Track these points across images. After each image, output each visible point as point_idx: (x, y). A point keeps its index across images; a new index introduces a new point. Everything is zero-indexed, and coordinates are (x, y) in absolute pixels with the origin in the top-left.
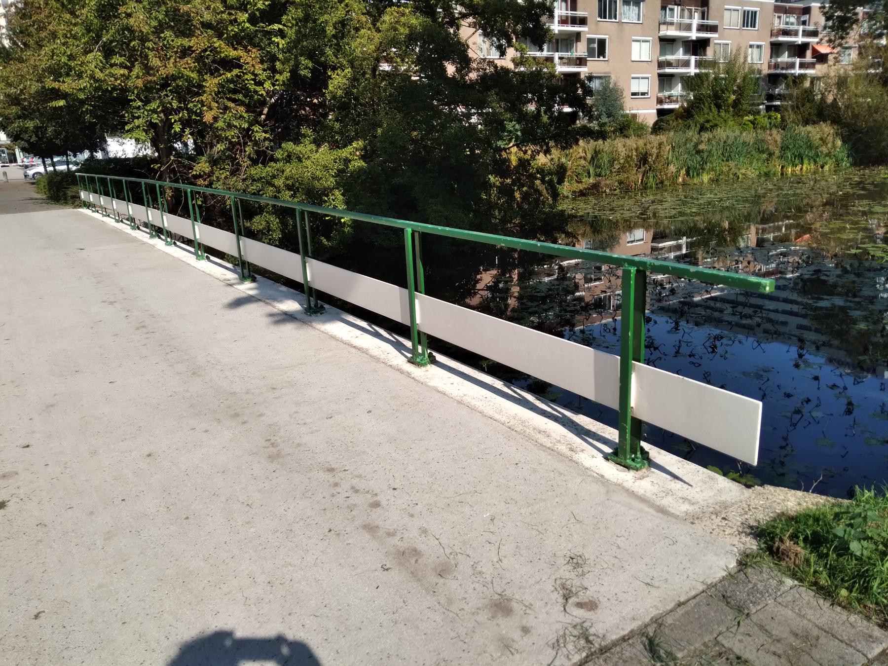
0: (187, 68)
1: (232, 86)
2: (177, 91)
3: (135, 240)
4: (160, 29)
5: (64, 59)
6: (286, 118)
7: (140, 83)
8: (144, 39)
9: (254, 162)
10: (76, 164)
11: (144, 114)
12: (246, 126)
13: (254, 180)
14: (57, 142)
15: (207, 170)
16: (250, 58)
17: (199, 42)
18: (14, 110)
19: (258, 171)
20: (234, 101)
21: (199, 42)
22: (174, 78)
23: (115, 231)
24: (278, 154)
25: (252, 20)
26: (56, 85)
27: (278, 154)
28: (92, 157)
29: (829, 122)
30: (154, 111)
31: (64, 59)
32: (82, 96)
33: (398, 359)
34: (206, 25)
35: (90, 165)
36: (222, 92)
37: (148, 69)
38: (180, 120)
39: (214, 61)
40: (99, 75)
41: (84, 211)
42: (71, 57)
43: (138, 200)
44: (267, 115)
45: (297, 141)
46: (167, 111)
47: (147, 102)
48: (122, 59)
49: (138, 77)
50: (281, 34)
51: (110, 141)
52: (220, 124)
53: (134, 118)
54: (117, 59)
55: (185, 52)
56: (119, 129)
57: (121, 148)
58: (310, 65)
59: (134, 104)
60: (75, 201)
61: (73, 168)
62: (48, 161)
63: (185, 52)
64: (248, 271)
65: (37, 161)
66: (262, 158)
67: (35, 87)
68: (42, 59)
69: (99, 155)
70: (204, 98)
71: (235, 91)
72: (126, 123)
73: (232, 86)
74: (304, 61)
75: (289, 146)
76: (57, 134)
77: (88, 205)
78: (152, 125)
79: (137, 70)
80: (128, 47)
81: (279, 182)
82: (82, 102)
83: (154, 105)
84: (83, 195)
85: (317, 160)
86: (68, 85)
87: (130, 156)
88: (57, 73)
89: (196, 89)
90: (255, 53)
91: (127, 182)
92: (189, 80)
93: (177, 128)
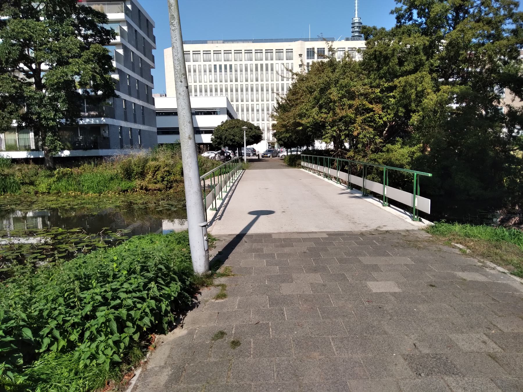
0: (350, 113)
1: (369, 119)
2: (345, 122)
3: (318, 178)
4: (341, 98)
5: (305, 111)
6: (397, 131)
7: (331, 120)
8: (335, 102)
9: (373, 152)
10: (300, 151)
11: (331, 131)
12: (372, 136)
13: (371, 160)
14: (295, 142)
15: (353, 155)
16: (377, 108)
17: (356, 102)
18: (284, 130)
19: (373, 156)
20: (369, 126)
21: (356, 102)
22: (345, 117)
23: (312, 176)
24: (384, 149)
25: (382, 91)
26: (300, 121)
27: (384, 149)
28: (307, 149)
29: (408, 146)
30: (335, 131)
31: (305, 111)
32: (308, 125)
33: (380, 205)
34: (362, 95)
35: (306, 152)
36: (364, 121)
37: (335, 114)
38: (344, 134)
39: (363, 109)
40: (316, 117)
41: (302, 169)
42: (307, 110)
43: (322, 164)
44: (387, 131)
45: (393, 144)
46: (341, 131)
47: (332, 127)
48: (326, 110)
49: (330, 117)
50: (394, 97)
51: (316, 141)
52: (361, 136)
53: (326, 133)
54: (324, 110)
55: (350, 106)
56: (320, 137)
57: (320, 145)
58: (404, 111)
59: (327, 128)
60: (299, 166)
61: (299, 153)
62: (289, 150)
63: (350, 106)
64: (352, 186)
65: (284, 149)
66: (377, 150)
67: (292, 121)
68: (296, 111)
69: (310, 148)
70: (355, 125)
71: (370, 122)
72: (323, 136)
73: (369, 119)
74: (401, 109)
75: (389, 146)
76: (296, 138)
77: (303, 167)
78: (333, 137)
79: (331, 114)
80: (327, 106)
81: (380, 161)
82: (308, 127)
83: (335, 128)
84: (302, 163)
85: (400, 152)
86: (304, 121)
87: (324, 149)
88: (301, 116)
89: (353, 122)
90: (380, 106)
91: (320, 158)
92: (350, 118)
93: (343, 138)
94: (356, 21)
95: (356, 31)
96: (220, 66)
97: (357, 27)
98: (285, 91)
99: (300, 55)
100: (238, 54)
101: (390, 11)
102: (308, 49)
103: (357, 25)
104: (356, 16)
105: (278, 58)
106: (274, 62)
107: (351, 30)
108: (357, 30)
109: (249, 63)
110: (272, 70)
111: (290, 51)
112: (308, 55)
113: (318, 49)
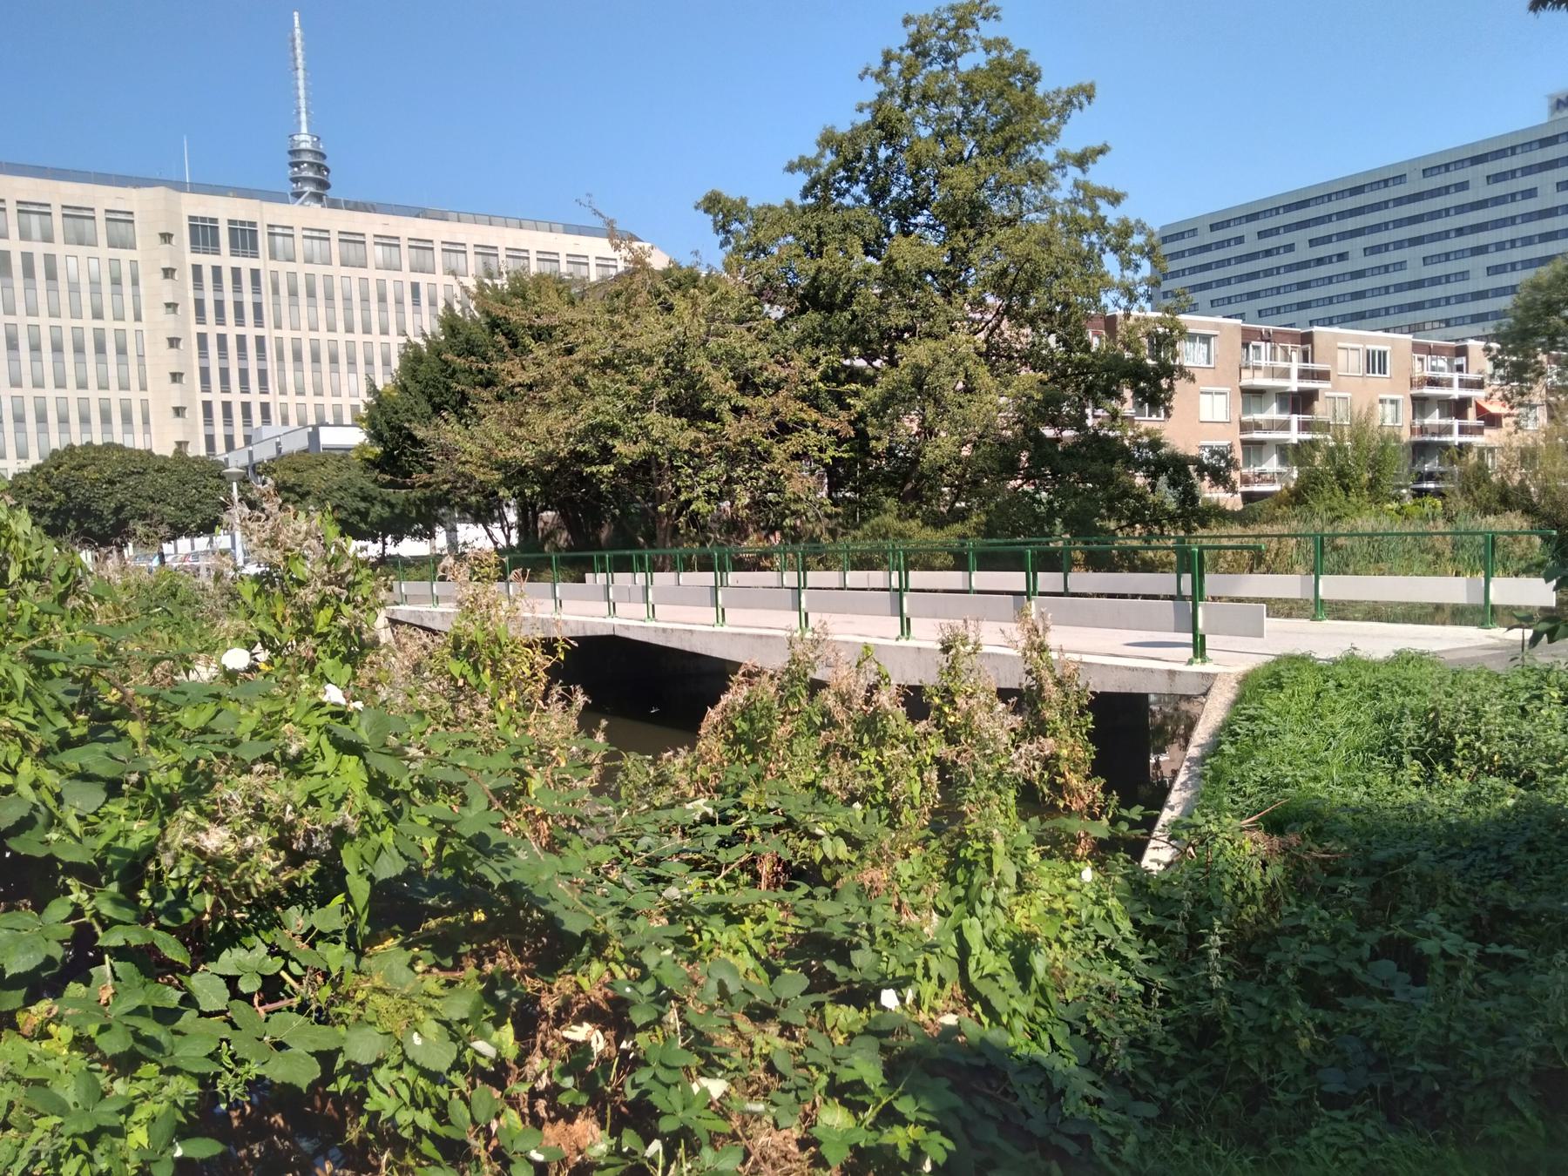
94: (303, 146)
95: (306, 179)
96: (217, 271)
97: (311, 164)
98: (396, 363)
99: (170, 236)
100: (351, 245)
101: (786, 164)
102: (191, 218)
103: (308, 158)
104: (304, 129)
105: (72, 236)
106: (59, 248)
107: (290, 172)
108: (311, 174)
109: (390, 277)
110: (51, 275)
111: (120, 219)
112: (194, 240)
113: (231, 222)
